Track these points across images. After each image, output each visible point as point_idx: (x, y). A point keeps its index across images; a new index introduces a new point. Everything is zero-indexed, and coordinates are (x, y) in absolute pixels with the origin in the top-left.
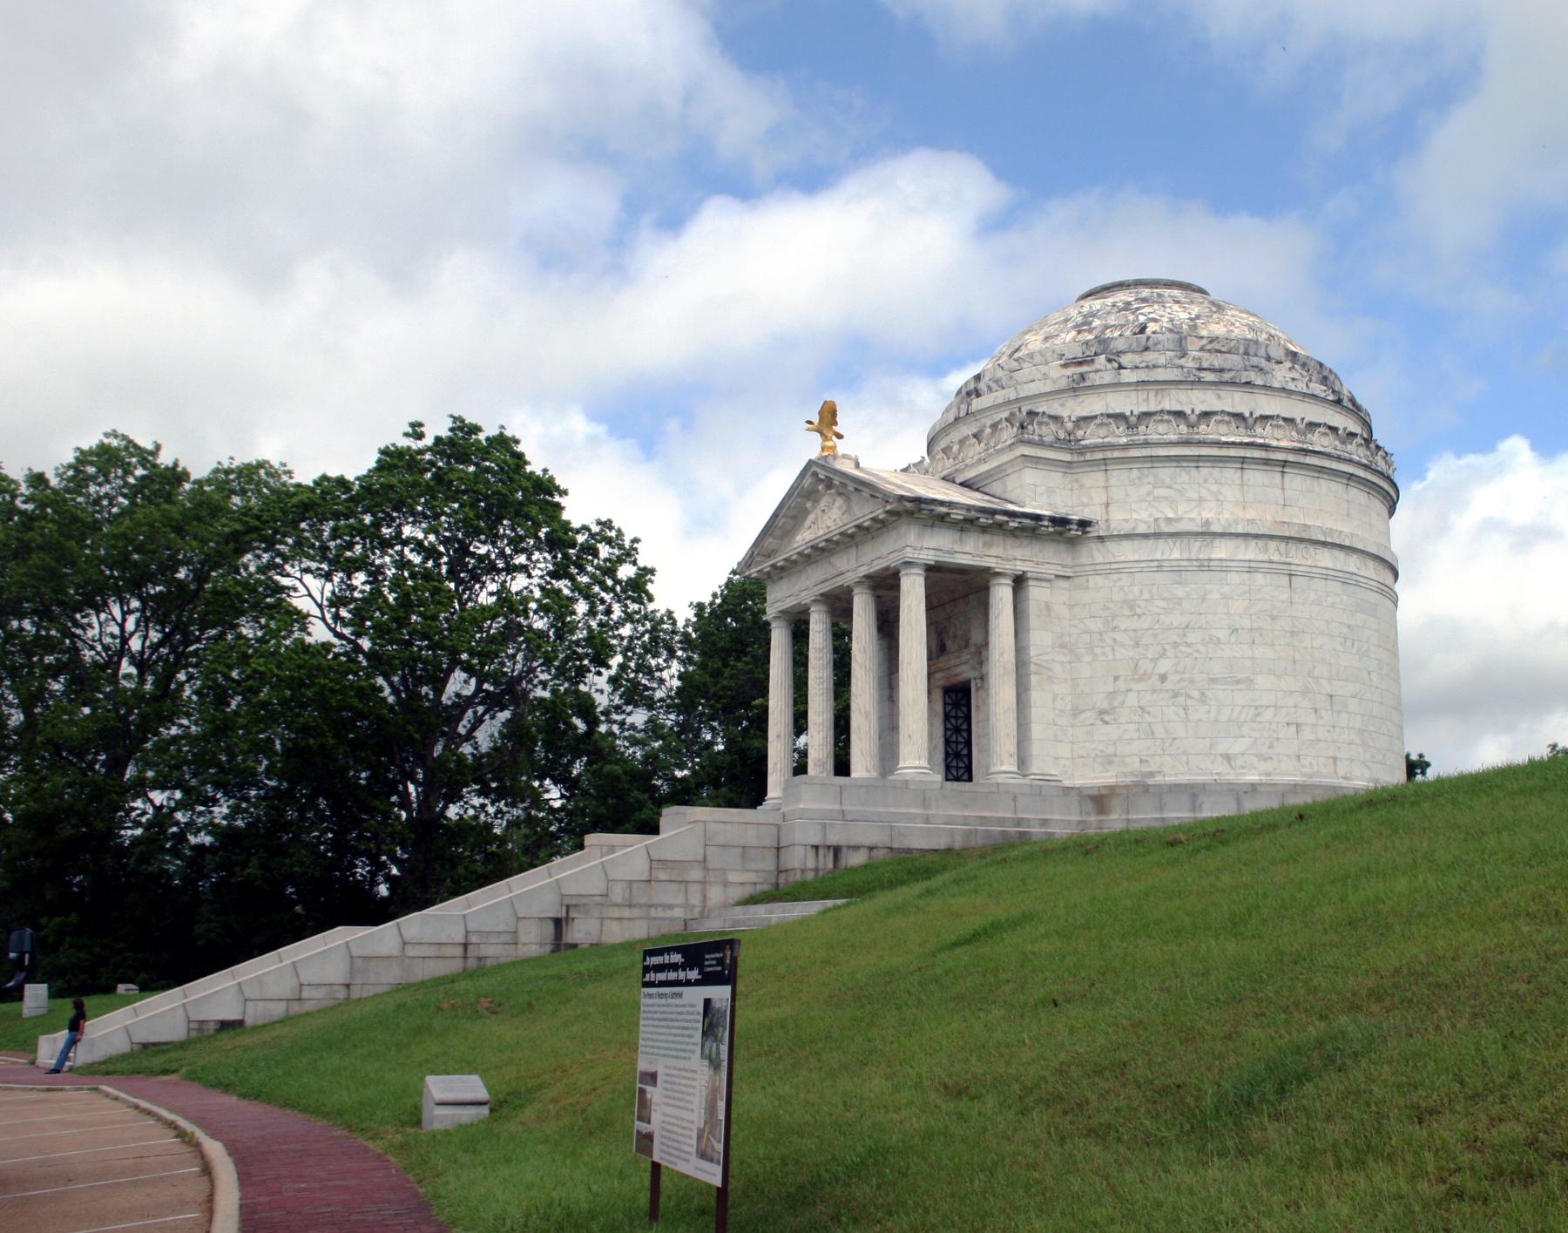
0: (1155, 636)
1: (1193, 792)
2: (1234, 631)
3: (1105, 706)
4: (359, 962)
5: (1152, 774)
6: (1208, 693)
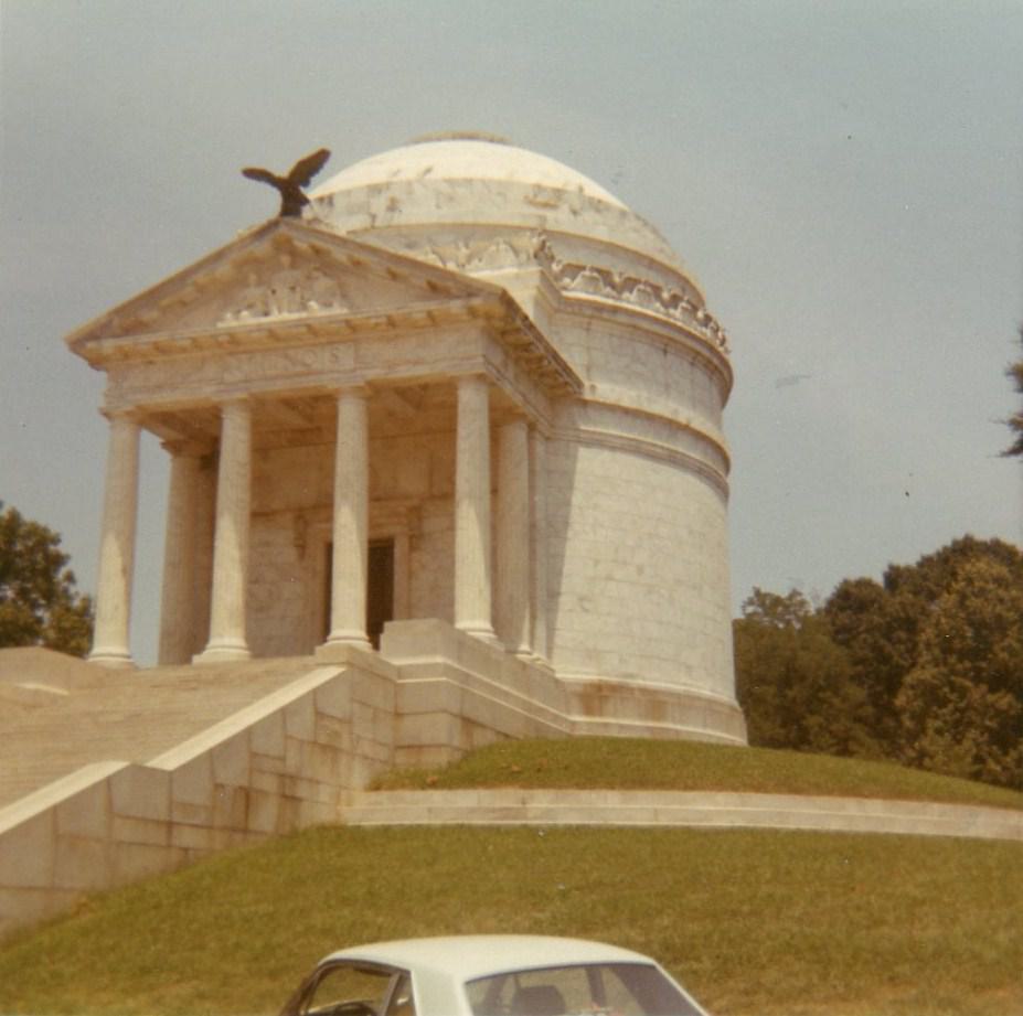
5: (631, 676)
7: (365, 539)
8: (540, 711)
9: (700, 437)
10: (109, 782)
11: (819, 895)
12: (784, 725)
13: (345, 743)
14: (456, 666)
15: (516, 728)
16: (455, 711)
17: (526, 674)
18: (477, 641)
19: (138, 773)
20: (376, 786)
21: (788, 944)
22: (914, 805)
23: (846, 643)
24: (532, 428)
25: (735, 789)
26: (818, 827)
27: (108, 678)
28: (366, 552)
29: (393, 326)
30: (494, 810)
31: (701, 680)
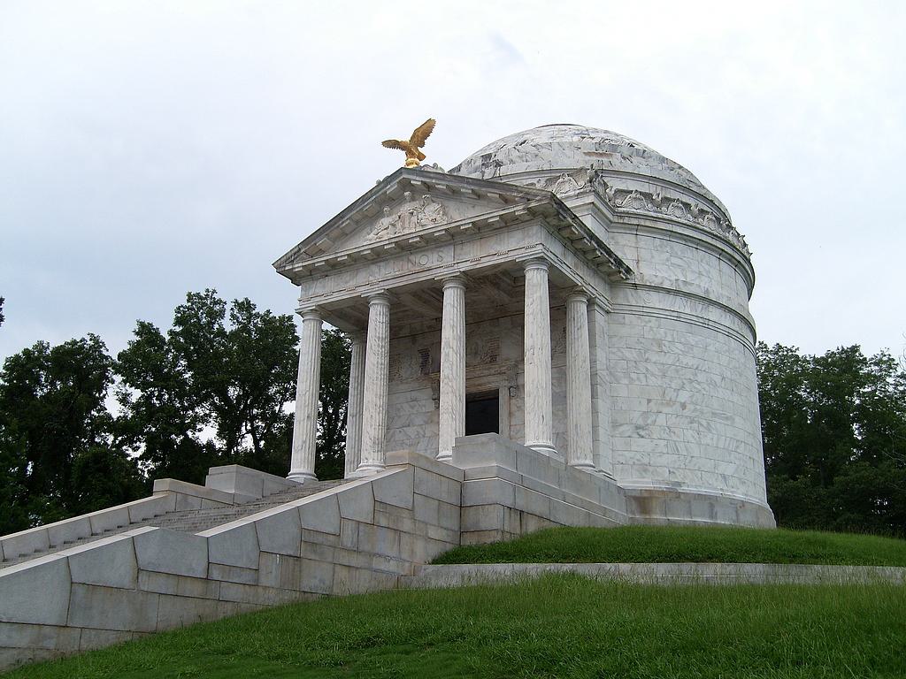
0: (677, 371)
1: (711, 502)
2: (723, 378)
3: (640, 422)
4: (80, 591)
5: (679, 484)
6: (712, 424)
16: (509, 503)
24: (591, 303)
29: (480, 231)
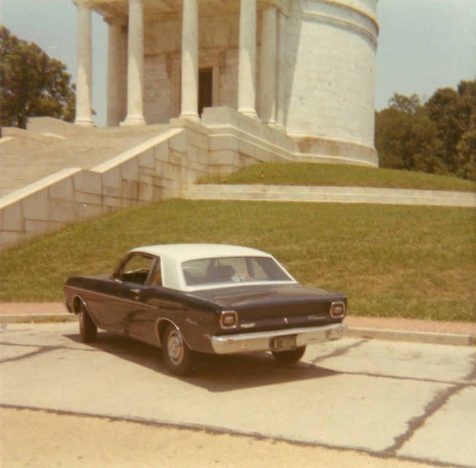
5: (323, 135)
7: (197, 68)
8: (279, 151)
9: (363, 16)
10: (72, 177)
11: (382, 231)
12: (403, 159)
13: (184, 163)
14: (237, 128)
15: (266, 159)
17: (272, 134)
18: (247, 118)
19: (86, 174)
20: (199, 182)
21: (362, 251)
22: (445, 193)
23: (436, 120)
24: (279, 11)
25: (363, 186)
26: (238, 199)
27: (82, 131)
28: (197, 75)
30: (250, 194)
31: (358, 138)
